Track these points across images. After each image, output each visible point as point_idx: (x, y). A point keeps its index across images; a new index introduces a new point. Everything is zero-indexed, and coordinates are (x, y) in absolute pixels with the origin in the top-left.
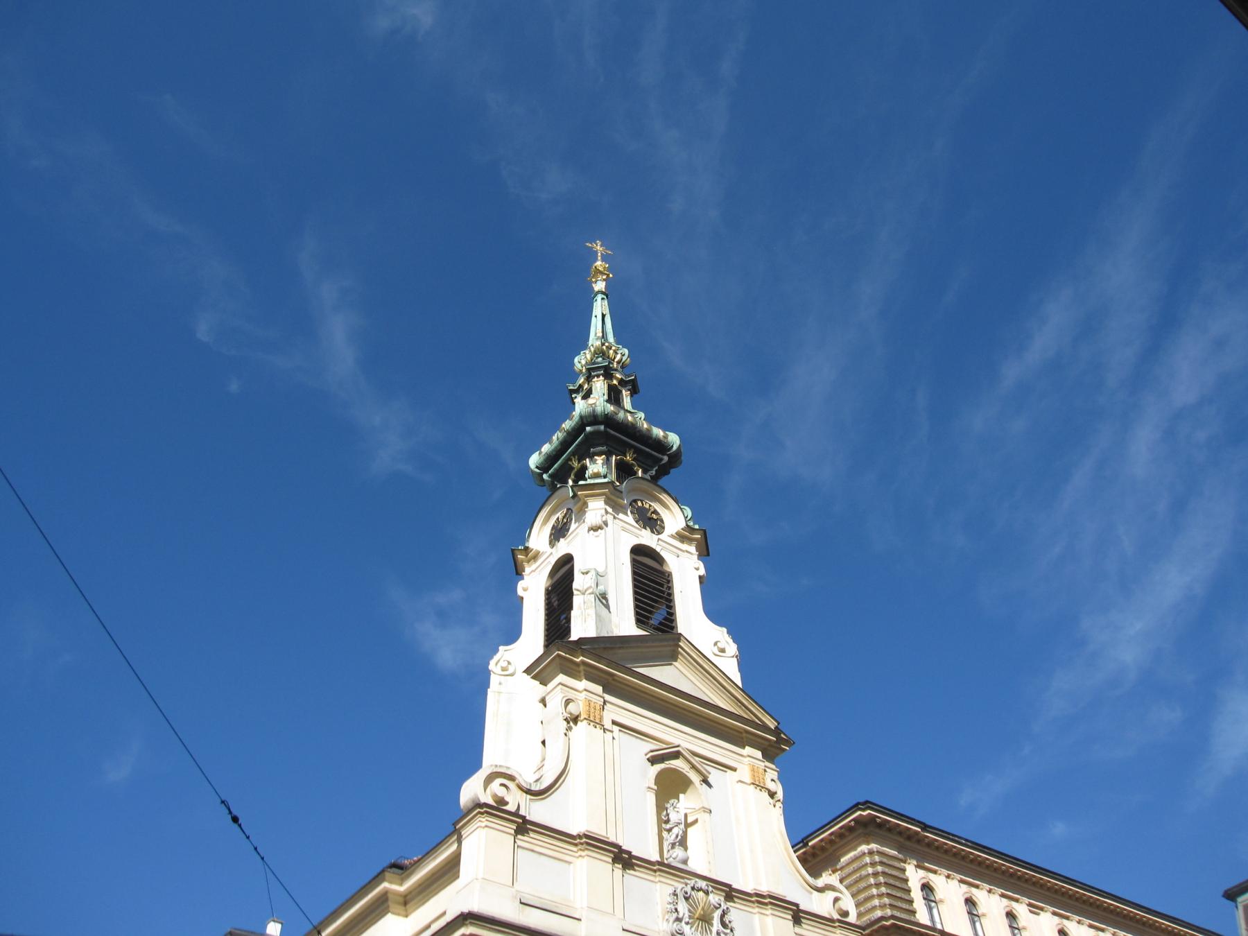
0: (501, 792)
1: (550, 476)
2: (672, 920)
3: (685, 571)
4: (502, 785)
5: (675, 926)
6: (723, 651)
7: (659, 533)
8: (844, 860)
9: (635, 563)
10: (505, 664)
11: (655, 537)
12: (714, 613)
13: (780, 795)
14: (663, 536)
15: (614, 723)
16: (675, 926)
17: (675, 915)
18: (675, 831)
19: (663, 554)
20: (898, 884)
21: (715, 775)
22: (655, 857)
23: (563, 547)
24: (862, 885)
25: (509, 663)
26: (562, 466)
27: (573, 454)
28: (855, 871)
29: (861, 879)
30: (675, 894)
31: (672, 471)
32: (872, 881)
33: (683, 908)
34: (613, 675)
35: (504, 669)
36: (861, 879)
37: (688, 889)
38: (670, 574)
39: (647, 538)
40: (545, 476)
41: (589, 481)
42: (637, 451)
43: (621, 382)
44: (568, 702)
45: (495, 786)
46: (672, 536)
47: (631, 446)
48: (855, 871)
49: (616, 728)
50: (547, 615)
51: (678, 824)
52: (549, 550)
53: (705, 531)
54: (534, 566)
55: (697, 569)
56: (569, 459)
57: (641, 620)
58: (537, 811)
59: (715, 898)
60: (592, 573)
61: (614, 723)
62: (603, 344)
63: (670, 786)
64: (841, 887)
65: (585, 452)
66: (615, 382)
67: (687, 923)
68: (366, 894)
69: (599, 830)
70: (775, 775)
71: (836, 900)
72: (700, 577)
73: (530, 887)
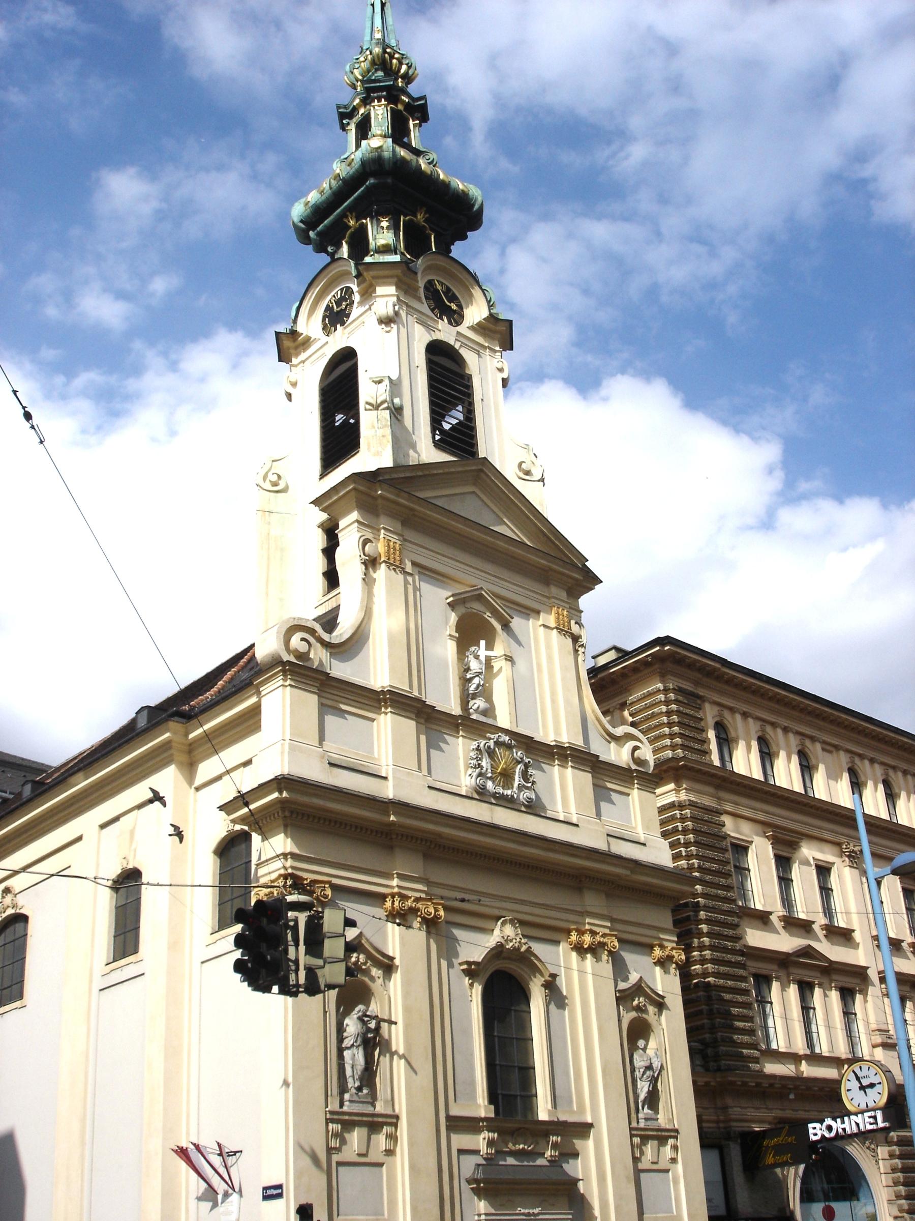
0: (303, 647)
1: (319, 234)
2: (475, 774)
4: (303, 639)
5: (480, 781)
6: (528, 473)
7: (458, 324)
9: (432, 366)
10: (275, 478)
14: (463, 329)
16: (480, 781)
17: (478, 771)
18: (476, 681)
19: (464, 353)
20: (692, 724)
22: (456, 710)
23: (340, 339)
24: (653, 723)
25: (279, 477)
27: (350, 209)
28: (647, 708)
29: (653, 716)
30: (478, 749)
32: (665, 719)
33: (485, 763)
35: (275, 484)
36: (653, 716)
37: (491, 744)
38: (470, 378)
39: (445, 332)
40: (312, 234)
43: (408, 106)
44: (366, 542)
45: (296, 641)
46: (472, 328)
48: (647, 708)
51: (478, 674)
52: (324, 338)
54: (303, 356)
55: (501, 370)
56: (344, 215)
58: (340, 670)
59: (518, 754)
60: (387, 382)
62: (385, 52)
63: (470, 632)
64: (640, 736)
66: (400, 107)
67: (490, 778)
68: (596, 1082)
69: (403, 686)
71: (636, 748)
72: (503, 380)
73: (335, 748)
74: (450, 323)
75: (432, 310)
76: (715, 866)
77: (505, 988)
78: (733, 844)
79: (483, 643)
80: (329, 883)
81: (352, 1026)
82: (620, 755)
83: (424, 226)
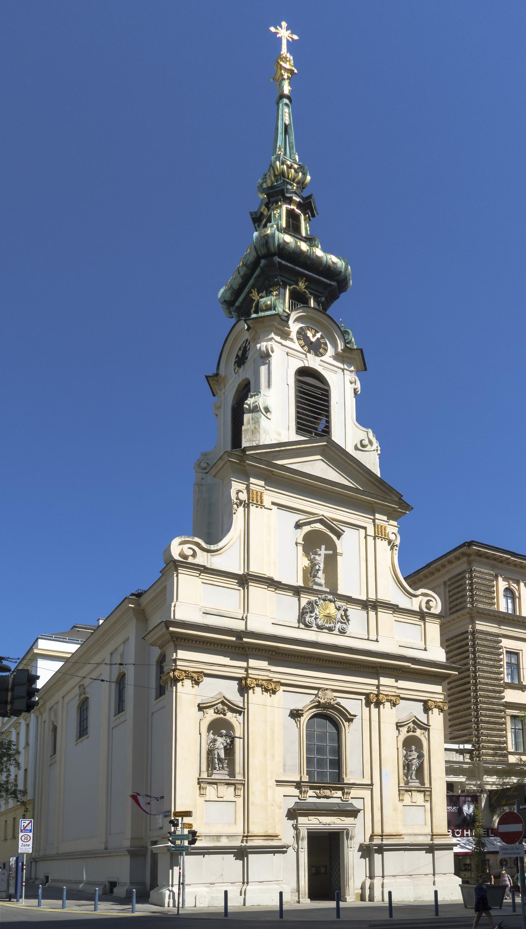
3: (343, 387)
7: (322, 355)
8: (502, 627)
9: (299, 383)
11: (318, 359)
12: (363, 419)
13: (398, 542)
15: (273, 503)
21: (348, 533)
26: (244, 299)
27: (253, 287)
31: (342, 295)
34: (272, 471)
41: (261, 314)
42: (309, 279)
47: (302, 275)
49: (274, 508)
50: (441, 635)
53: (361, 350)
57: (301, 428)
61: (273, 503)
63: (311, 543)
65: (305, 277)
70: (396, 530)
73: (211, 606)
74: (316, 355)
75: (302, 347)
76: (491, 663)
77: (328, 719)
78: (507, 652)
79: (323, 547)
80: (202, 672)
81: (221, 742)
82: (415, 604)
83: (305, 292)
